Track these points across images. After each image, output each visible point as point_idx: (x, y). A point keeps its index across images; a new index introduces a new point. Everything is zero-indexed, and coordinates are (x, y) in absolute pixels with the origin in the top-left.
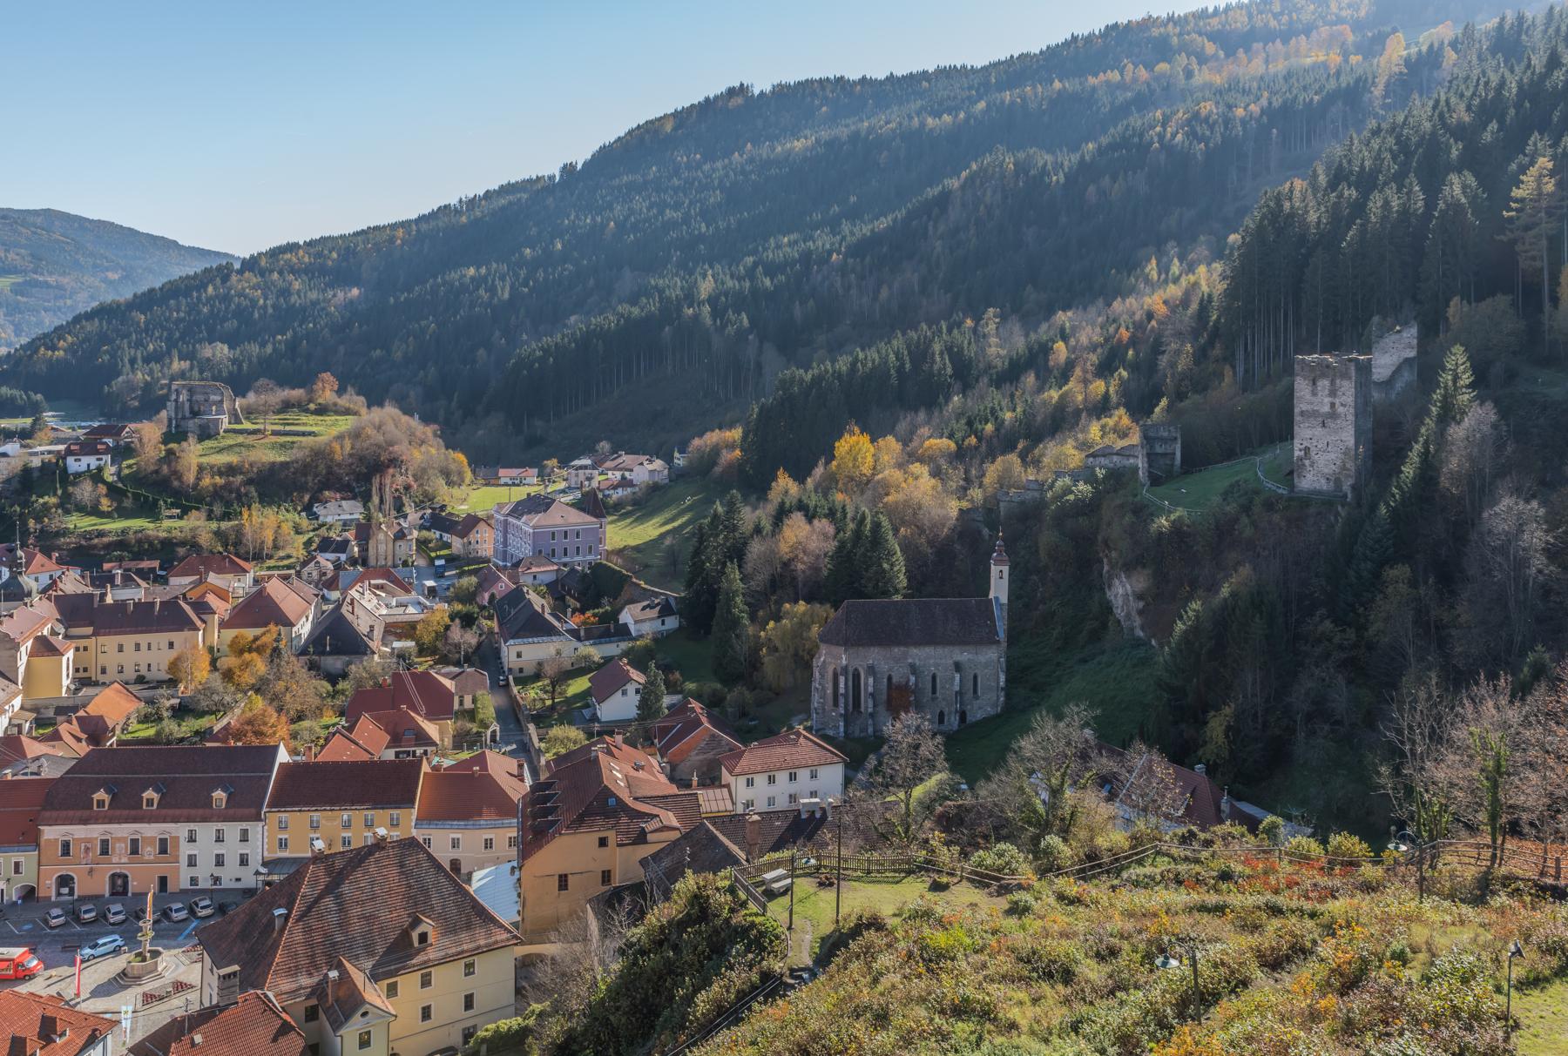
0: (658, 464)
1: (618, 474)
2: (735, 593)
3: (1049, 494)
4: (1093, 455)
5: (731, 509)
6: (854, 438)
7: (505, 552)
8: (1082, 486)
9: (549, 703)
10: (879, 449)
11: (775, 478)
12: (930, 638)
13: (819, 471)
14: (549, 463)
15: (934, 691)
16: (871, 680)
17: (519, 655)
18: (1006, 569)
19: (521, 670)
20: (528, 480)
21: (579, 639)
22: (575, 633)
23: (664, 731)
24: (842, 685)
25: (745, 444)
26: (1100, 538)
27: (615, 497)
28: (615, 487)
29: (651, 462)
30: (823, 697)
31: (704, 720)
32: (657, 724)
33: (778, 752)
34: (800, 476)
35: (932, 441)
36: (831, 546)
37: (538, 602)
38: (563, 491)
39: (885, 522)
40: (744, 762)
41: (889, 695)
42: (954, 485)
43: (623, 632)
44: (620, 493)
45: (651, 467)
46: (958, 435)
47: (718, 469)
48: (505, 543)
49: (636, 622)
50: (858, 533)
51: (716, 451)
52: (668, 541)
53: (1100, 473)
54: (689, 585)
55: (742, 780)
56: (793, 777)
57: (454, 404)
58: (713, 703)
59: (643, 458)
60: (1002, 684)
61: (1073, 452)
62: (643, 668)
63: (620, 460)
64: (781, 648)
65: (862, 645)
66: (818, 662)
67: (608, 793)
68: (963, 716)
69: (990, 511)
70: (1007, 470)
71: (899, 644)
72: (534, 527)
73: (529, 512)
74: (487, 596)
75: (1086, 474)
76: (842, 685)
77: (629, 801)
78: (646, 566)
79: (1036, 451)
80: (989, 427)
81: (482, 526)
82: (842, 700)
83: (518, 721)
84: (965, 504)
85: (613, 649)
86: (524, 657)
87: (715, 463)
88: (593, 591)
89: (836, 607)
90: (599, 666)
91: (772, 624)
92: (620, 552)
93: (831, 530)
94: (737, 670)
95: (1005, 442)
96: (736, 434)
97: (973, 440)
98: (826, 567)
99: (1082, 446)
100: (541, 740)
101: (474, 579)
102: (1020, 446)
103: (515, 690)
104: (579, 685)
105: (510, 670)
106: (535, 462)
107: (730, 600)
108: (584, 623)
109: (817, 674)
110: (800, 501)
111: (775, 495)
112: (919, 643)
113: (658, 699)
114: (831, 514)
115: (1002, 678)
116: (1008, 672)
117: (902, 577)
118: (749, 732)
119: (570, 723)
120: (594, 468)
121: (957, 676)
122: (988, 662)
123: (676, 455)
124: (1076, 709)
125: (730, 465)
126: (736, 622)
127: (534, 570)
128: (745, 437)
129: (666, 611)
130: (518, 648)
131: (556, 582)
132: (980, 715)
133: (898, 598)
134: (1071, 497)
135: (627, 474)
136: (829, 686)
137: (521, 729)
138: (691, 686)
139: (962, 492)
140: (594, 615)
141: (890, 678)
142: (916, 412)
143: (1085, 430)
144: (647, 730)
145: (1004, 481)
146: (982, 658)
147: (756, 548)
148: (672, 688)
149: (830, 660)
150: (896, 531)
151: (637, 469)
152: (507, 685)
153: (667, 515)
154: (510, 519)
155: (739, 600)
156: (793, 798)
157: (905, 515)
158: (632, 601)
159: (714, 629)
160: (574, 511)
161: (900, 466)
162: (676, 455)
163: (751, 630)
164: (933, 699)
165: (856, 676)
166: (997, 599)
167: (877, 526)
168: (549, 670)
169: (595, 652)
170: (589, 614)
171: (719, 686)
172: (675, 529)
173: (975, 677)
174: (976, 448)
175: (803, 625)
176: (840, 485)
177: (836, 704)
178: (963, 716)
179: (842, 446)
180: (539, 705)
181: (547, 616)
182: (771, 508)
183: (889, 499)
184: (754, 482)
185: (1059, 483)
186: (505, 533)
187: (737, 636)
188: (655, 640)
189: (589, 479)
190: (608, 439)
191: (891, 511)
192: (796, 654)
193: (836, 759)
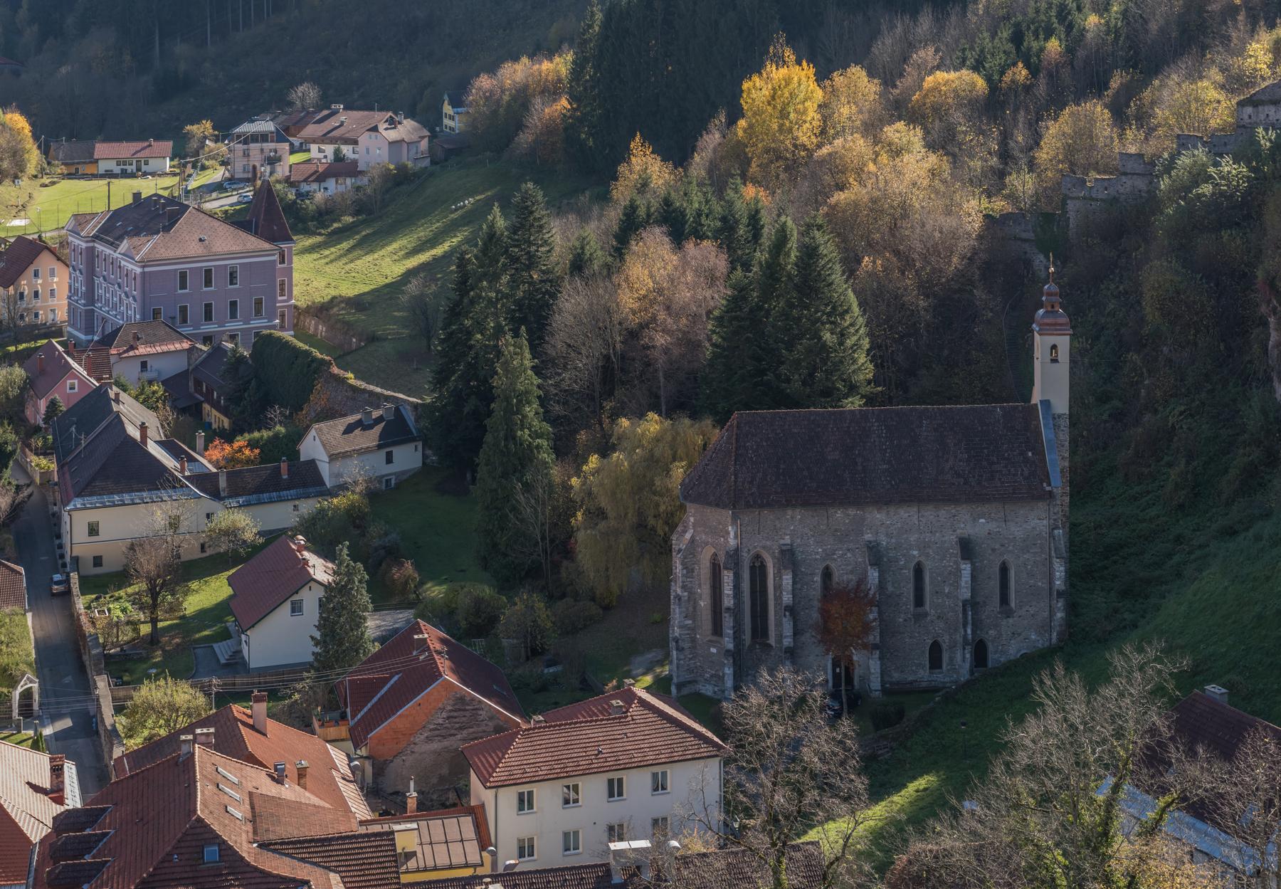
0: (407, 129)
1: (329, 149)
2: (523, 398)
3: (1164, 184)
4: (1253, 102)
5: (524, 221)
6: (783, 71)
7: (90, 315)
8: (1228, 166)
9: (145, 629)
10: (834, 92)
11: (623, 155)
12: (911, 489)
13: (711, 140)
14: (194, 128)
15: (919, 601)
16: (787, 579)
17: (93, 530)
18: (1064, 342)
19: (98, 561)
20: (154, 165)
21: (216, 495)
22: (206, 482)
23: (364, 690)
24: (728, 590)
25: (576, 85)
26: (1260, 274)
27: (319, 196)
28: (321, 178)
29: (393, 123)
30: (692, 614)
31: (444, 664)
32: (345, 677)
33: (588, 734)
34: (678, 154)
35: (941, 76)
36: (717, 297)
37: (137, 418)
38: (219, 187)
39: (828, 248)
40: (512, 758)
41: (825, 613)
42: (977, 164)
43: (306, 479)
44: (333, 187)
45: (392, 135)
46: (991, 64)
47: (525, 138)
48: (90, 297)
49: (333, 458)
50: (772, 270)
51: (523, 97)
52: (413, 287)
53: (1265, 138)
54: (441, 379)
55: (508, 797)
56: (615, 789)
57: (23, 13)
58: (470, 629)
59: (380, 118)
60: (1059, 583)
61: (1213, 94)
62: (327, 553)
63: (333, 122)
64: (611, 514)
65: (769, 505)
66: (681, 541)
67: (203, 835)
68: (980, 651)
69: (1048, 218)
70: (1084, 134)
71: (845, 501)
72: (144, 263)
73: (137, 233)
74: (43, 405)
75: (1232, 140)
76: (728, 590)
77: (246, 849)
78: (373, 339)
79: (1147, 94)
80: (1054, 46)
81: (45, 262)
82: (728, 622)
83: (82, 669)
84: (999, 205)
85: (284, 514)
86: (104, 533)
87: (520, 126)
88: (252, 392)
89: (721, 422)
90: (255, 549)
91: (594, 461)
92: (321, 310)
93: (720, 263)
94: (534, 560)
95: (1084, 76)
96: (558, 66)
97: (1020, 73)
98: (709, 336)
99: (1235, 82)
100: (119, 710)
101: (18, 372)
102: (1115, 83)
103: (80, 603)
104: (209, 593)
105: (76, 560)
106: (170, 130)
107: (513, 411)
108: (231, 460)
109: (678, 568)
110: (667, 202)
111: (622, 192)
112: (884, 501)
113: (357, 622)
114: (726, 233)
115: (1060, 570)
116: (1074, 550)
117: (862, 358)
118: (544, 688)
119: (176, 675)
120: (280, 138)
121: (966, 568)
122: (1029, 535)
123: (447, 109)
124: (1137, 659)
125: (550, 129)
126: (523, 459)
127: (142, 350)
128: (577, 69)
129: (395, 433)
130: (93, 516)
131: (183, 375)
132: (1014, 650)
133: (853, 404)
134: (1207, 189)
135: (346, 150)
136: (704, 591)
137: (87, 688)
138: (435, 591)
139: (995, 182)
140: (252, 445)
141: (827, 574)
142: (914, 14)
143: (1241, 52)
144: (337, 691)
145: (1078, 154)
146: (1017, 530)
147: (572, 303)
148: (385, 596)
149: (707, 535)
150: (851, 263)
151: (365, 139)
152: (68, 593)
153: (422, 233)
154: (100, 247)
155: (530, 410)
156: (570, 841)
157: (879, 228)
158: (329, 414)
159: (482, 471)
160: (225, 230)
161: (872, 129)
162: (447, 109)
163: (556, 472)
164: (919, 617)
165: (758, 570)
166: (1046, 404)
167: (810, 253)
168: (148, 563)
169: (245, 521)
170: (240, 442)
171: (487, 591)
172: (436, 260)
173: (1004, 570)
174: (1027, 89)
175: (655, 463)
176: (754, 168)
177: (717, 630)
178: (980, 651)
179: (756, 90)
180: (126, 635)
181: (154, 449)
182: (613, 216)
183: (840, 197)
184: (582, 164)
185: (1184, 160)
186: (91, 274)
187: (528, 487)
188: (372, 495)
189: (273, 161)
190: (315, 80)
191: (842, 224)
192: (641, 525)
193: (705, 749)
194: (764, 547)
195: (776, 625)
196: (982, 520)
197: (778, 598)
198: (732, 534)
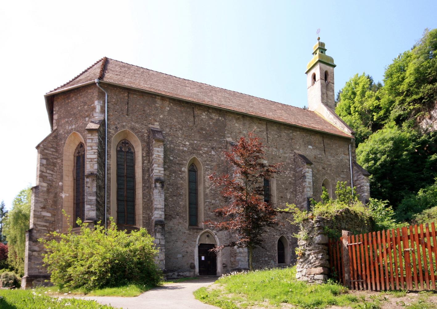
82: (91, 187)
145: (67, 212)
194: (133, 129)
195: (144, 208)
196: (310, 147)
197: (147, 171)
198: (98, 108)
